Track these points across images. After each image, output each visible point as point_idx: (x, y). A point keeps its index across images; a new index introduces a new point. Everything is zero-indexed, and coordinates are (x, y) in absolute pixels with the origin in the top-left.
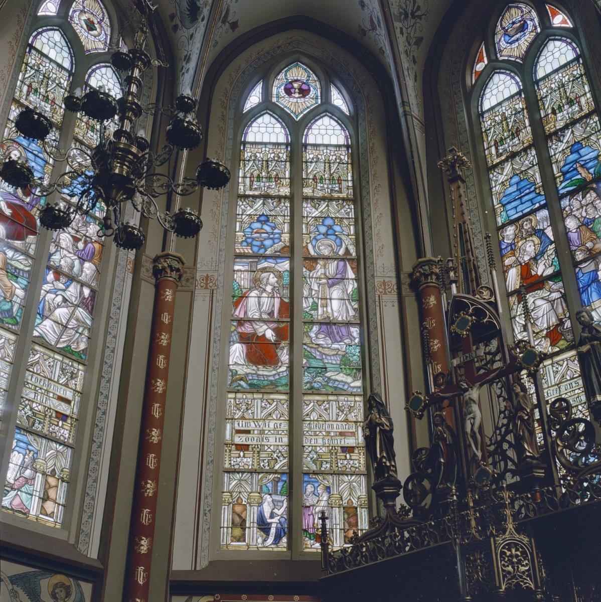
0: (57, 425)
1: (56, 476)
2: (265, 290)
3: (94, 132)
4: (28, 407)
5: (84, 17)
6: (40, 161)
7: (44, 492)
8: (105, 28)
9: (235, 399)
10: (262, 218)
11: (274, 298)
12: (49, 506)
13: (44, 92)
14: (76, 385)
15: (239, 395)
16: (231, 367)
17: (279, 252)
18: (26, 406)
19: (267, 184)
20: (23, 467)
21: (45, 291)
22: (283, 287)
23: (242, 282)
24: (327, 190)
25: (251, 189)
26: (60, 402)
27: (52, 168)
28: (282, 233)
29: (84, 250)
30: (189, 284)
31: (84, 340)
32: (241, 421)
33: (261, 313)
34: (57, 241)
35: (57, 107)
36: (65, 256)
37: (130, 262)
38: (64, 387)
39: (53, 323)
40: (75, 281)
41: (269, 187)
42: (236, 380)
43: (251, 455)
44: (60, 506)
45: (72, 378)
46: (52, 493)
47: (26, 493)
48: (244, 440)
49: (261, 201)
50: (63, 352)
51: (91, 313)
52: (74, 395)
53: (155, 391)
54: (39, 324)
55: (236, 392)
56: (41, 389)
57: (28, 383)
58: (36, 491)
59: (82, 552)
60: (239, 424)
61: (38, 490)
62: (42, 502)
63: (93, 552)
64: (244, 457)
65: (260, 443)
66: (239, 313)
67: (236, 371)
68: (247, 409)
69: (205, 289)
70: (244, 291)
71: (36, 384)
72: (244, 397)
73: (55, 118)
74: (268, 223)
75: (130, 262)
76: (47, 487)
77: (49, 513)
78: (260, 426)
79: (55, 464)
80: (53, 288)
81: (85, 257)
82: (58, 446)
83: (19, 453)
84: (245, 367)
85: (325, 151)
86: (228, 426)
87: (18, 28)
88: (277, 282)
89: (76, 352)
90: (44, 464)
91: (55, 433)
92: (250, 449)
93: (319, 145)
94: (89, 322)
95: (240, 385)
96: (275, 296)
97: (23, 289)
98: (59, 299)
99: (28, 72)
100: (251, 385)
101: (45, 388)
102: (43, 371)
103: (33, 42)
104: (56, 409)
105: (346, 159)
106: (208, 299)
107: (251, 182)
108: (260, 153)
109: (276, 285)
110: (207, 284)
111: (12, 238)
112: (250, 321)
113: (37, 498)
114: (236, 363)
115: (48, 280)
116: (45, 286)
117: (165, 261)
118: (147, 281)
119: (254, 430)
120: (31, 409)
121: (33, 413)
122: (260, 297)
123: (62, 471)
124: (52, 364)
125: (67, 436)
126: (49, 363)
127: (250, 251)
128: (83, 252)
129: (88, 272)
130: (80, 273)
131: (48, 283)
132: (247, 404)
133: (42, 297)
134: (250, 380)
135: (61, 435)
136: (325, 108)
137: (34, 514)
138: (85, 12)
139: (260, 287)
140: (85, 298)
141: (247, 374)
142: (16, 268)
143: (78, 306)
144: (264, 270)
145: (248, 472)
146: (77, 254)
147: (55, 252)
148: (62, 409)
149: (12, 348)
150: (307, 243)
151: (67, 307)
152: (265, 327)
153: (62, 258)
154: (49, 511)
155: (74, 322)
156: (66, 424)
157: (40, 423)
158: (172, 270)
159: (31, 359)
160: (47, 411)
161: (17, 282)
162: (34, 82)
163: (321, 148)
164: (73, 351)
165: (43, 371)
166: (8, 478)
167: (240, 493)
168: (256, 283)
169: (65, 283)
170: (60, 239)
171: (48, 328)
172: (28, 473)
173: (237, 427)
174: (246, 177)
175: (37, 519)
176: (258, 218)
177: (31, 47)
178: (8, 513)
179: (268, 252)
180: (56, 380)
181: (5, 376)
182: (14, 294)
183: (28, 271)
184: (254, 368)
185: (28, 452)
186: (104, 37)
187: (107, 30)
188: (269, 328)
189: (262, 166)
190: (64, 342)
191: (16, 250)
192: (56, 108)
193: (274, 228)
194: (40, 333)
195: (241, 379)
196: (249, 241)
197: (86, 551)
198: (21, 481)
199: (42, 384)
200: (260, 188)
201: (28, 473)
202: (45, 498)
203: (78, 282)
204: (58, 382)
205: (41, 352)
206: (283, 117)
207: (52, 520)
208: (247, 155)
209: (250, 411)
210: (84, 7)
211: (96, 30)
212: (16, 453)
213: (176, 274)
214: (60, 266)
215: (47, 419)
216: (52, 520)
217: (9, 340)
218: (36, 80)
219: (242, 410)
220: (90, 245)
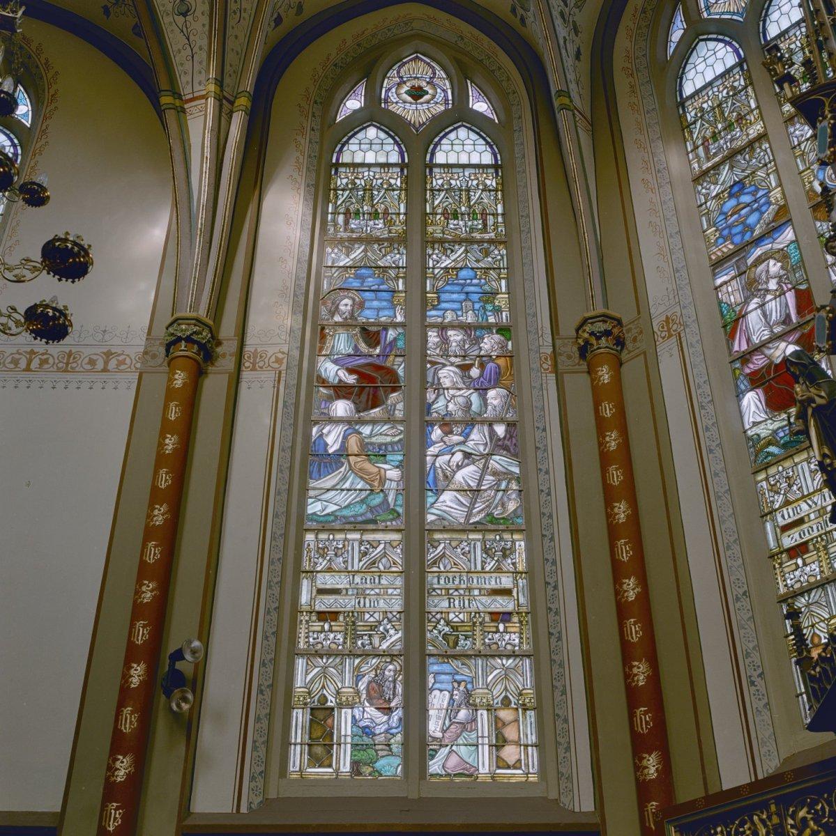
0: (498, 631)
1: (513, 705)
2: (767, 291)
3: (458, 219)
4: (442, 622)
5: (405, 88)
6: (384, 294)
7: (497, 735)
8: (441, 84)
9: (767, 479)
10: (736, 189)
11: (784, 294)
12: (510, 753)
13: (468, 209)
14: (514, 564)
15: (772, 471)
16: (750, 433)
17: (773, 221)
18: (438, 622)
19: (729, 137)
20: (452, 709)
21: (433, 456)
22: (794, 270)
23: (732, 297)
24: (464, 229)
25: (708, 159)
26: (493, 597)
27: (404, 295)
28: (770, 192)
29: (481, 375)
30: (638, 344)
31: (514, 496)
32: (784, 510)
33: (771, 327)
34: (436, 382)
35: (394, 216)
36: (454, 396)
37: (546, 359)
38: (494, 575)
39: (455, 493)
40: (478, 422)
41: (732, 140)
42: (761, 450)
43: (517, 630)
44: (530, 748)
45: (505, 556)
46: (510, 733)
47: (466, 745)
48: (798, 538)
49: (363, 247)
50: (479, 527)
51: (515, 455)
52: (515, 579)
53: (614, 522)
54: (435, 503)
55: (766, 469)
56: (456, 590)
57: (434, 590)
58: (483, 737)
59: (566, 807)
60: (783, 516)
61: (486, 734)
62: (497, 750)
63: (585, 803)
64: (805, 564)
65: (824, 531)
66: (740, 345)
67: (758, 435)
68: (790, 486)
69: (251, 370)
70: (738, 309)
71: (448, 586)
72: (780, 468)
73: (394, 231)
74: (746, 191)
75: (546, 359)
76: (498, 726)
77: (511, 763)
78: (816, 504)
79: (506, 689)
80: (445, 446)
81: (486, 385)
82: (504, 661)
83: (441, 691)
84: (770, 421)
85: (461, 174)
86: (769, 526)
87: (298, 154)
88: (782, 268)
89: (503, 518)
90: (488, 694)
91: (496, 643)
92: (811, 547)
93: (787, 31)
94: (516, 470)
95: (769, 454)
96: (785, 289)
97: (397, 467)
98: (458, 457)
99: (340, 196)
100: (785, 446)
101: (464, 586)
102: (394, 564)
103: (338, 159)
104: (490, 610)
105: (494, 184)
106: (676, 351)
107: (707, 150)
108: (456, 180)
109: (782, 272)
110: (669, 330)
111: (366, 409)
112: (759, 349)
113: (486, 747)
114: (754, 423)
115: (434, 439)
116: (432, 449)
117: (584, 331)
118: (570, 373)
119: (808, 515)
120: (448, 623)
121: (452, 627)
122: (764, 305)
123: (520, 694)
124: (467, 549)
125: (517, 641)
126: (463, 549)
127: (731, 247)
128: (482, 379)
129: (495, 402)
130: (484, 409)
131: (435, 443)
132: (788, 477)
133: (429, 466)
134: (781, 438)
135: (506, 644)
136: (458, 116)
137: (487, 771)
138: (405, 83)
139: (760, 290)
140: (500, 440)
141: (775, 432)
142: (380, 445)
143: (492, 455)
144: (759, 261)
145: (817, 587)
146: (472, 385)
147: (436, 399)
148: (498, 606)
149: (399, 551)
150: (810, 183)
151: (473, 463)
152: (783, 345)
153: (449, 401)
154: (511, 761)
155: (489, 478)
156: (511, 625)
157: (466, 637)
158: (598, 338)
159: (432, 555)
160: (475, 617)
161: (386, 463)
162: (352, 203)
163: (791, 33)
164: (497, 519)
165: (455, 564)
166: (431, 732)
167: (813, 626)
168: (753, 288)
169: (462, 432)
170: (439, 379)
171: (449, 503)
172: (463, 714)
173: (781, 522)
174: (437, 214)
175: (493, 778)
176: (729, 193)
177: (338, 165)
178: (444, 783)
179: (757, 232)
180: (479, 568)
181: (395, 593)
182: (386, 479)
183: (400, 440)
184: (784, 416)
185: (456, 685)
186: (442, 95)
187: (445, 85)
188: (790, 343)
189: (460, 198)
190: (479, 512)
191: (374, 422)
192: (392, 219)
193: (754, 193)
194: (437, 515)
195: (769, 444)
196: (726, 232)
197: (572, 804)
198: (454, 730)
199: (457, 582)
200: (720, 148)
201: (463, 714)
202: (500, 743)
203: (482, 422)
204: (483, 571)
205: (446, 539)
206: (395, 127)
207: (521, 772)
208: (438, 183)
209: (795, 488)
210: (402, 78)
211: (427, 93)
212: (436, 692)
213: (607, 340)
214: (449, 414)
215: (478, 629)
216: (521, 772)
217: (390, 543)
218: (354, 200)
219: (782, 492)
220: (490, 366)
